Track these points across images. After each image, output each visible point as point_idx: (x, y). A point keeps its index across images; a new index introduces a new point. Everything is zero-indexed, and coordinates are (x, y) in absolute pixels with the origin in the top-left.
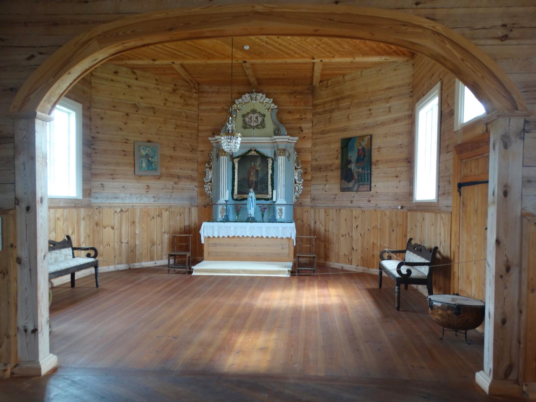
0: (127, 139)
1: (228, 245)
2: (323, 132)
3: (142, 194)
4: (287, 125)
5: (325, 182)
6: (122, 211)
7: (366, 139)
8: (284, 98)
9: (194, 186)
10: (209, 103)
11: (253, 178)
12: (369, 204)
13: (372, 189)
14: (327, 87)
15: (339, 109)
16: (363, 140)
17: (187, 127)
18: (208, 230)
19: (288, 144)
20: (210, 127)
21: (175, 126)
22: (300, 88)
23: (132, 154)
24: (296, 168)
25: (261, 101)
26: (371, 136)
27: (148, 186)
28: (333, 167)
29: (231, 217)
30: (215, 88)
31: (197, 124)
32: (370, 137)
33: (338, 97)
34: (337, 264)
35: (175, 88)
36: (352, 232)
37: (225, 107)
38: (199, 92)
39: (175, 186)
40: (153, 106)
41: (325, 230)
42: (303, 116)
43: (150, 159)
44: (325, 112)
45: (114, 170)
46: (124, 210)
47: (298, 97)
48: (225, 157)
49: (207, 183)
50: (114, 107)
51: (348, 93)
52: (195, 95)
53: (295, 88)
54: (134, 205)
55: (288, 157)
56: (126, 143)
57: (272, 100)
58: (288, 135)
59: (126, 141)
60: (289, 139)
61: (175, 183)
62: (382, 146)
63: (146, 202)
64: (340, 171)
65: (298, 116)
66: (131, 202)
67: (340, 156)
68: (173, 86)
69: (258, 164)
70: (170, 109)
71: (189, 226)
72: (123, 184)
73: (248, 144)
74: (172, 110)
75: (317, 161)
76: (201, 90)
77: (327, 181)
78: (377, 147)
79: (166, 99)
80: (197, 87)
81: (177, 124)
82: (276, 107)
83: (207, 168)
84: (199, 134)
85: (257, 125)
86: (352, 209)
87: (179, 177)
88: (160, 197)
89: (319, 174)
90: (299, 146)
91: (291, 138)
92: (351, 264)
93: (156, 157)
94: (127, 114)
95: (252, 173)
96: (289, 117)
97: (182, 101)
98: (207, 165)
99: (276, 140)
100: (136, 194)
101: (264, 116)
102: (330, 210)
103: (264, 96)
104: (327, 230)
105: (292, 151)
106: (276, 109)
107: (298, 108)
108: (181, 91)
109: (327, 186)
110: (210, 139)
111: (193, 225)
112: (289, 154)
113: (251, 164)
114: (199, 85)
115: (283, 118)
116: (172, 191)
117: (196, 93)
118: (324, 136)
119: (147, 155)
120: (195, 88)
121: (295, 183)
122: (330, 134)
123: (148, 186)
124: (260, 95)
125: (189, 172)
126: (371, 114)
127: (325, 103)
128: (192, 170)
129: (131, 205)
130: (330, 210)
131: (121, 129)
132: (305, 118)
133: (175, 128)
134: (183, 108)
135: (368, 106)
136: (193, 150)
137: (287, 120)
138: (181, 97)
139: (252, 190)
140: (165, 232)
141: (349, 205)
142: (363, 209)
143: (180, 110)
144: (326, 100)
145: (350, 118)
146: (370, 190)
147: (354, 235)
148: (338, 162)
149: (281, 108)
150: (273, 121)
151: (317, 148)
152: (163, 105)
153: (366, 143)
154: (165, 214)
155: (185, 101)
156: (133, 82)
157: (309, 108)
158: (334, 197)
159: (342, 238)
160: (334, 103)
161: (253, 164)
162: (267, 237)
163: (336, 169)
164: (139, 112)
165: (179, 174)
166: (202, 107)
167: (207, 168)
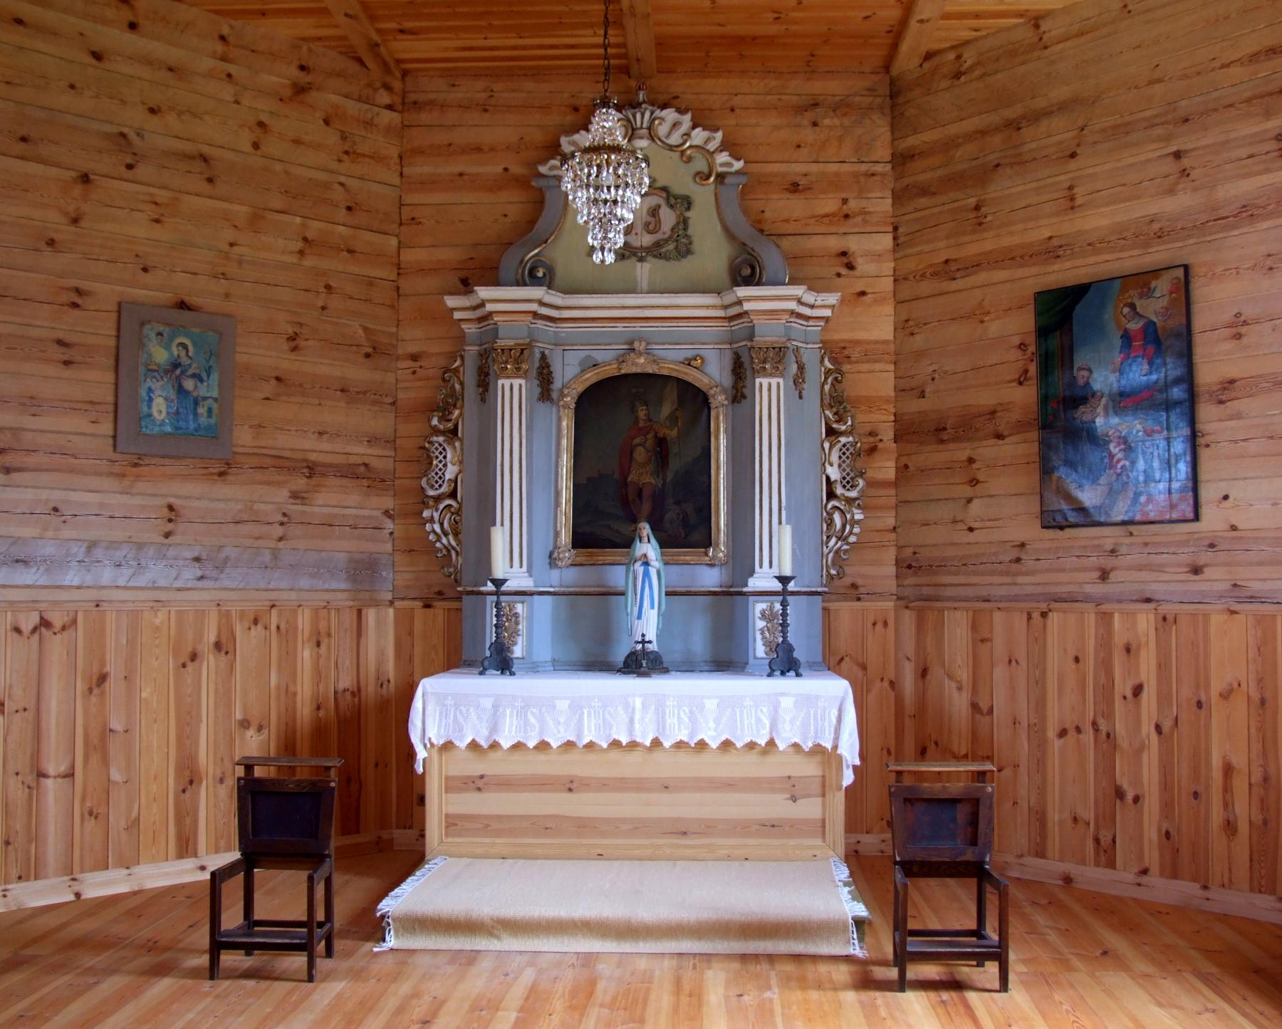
0: (78, 291)
1: (570, 785)
2: (947, 270)
3: (141, 546)
4: (786, 243)
5: (968, 491)
6: (45, 623)
7: (1162, 286)
8: (763, 128)
9: (378, 513)
10: (448, 150)
11: (643, 476)
12: (1197, 585)
13: (1205, 511)
14: (958, 75)
15: (1020, 162)
16: (1147, 293)
17: (350, 251)
18: (448, 714)
19: (798, 325)
20: (448, 255)
21: (300, 245)
22: (832, 87)
23: (111, 408)
24: (831, 432)
25: (675, 139)
26: (1186, 268)
27: (171, 508)
28: (1002, 423)
29: (1201, 617)
30: (472, 90)
31: (394, 242)
32: (1180, 273)
33: (1010, 113)
34: (1040, 862)
35: (304, 78)
36: (1109, 716)
37: (516, 169)
38: (405, 105)
39: (295, 508)
40: (206, 150)
41: (975, 707)
42: (853, 205)
43: (189, 384)
44: (955, 181)
45: (16, 431)
46: (57, 619)
47: (827, 122)
48: (516, 382)
49: (438, 499)
50: (23, 139)
51: (1061, 93)
52: (387, 117)
53: (818, 87)
54: (105, 595)
55: (799, 380)
56: (75, 305)
57: (719, 135)
58: (794, 281)
59: (77, 299)
60: (800, 302)
61: (295, 496)
62: (1249, 312)
63: (162, 583)
64: (1034, 435)
65: (829, 204)
66: (89, 580)
67: (1033, 369)
68: (294, 72)
69: (666, 410)
70: (278, 167)
71: (357, 692)
72: (57, 496)
73: (620, 327)
74: (286, 172)
75: (922, 395)
76: (412, 97)
77: (974, 482)
78: (1227, 316)
79: (261, 124)
80: (397, 85)
81: (310, 236)
82: (738, 165)
83: (436, 431)
84: (405, 285)
85: (658, 245)
86: (1104, 607)
87: (312, 470)
88: (226, 560)
89: (933, 455)
90: (840, 335)
91: (810, 298)
92: (1111, 864)
93: (215, 376)
94: (85, 179)
95: (640, 455)
96: (795, 207)
97: (331, 138)
98: (435, 422)
99: (747, 306)
100: (113, 545)
101: (687, 202)
102: (998, 616)
103: (687, 119)
104: (984, 706)
105: (811, 354)
106: (738, 173)
107: (833, 168)
108: (327, 98)
109: (976, 507)
110: (451, 302)
111: (370, 689)
112: (801, 368)
113: (633, 409)
114: (405, 73)
115: (768, 214)
116: (279, 531)
117: (390, 107)
118: (954, 285)
119: (176, 365)
120: (387, 87)
121: (831, 495)
122: (982, 277)
123: (171, 508)
124: (670, 115)
125: (360, 451)
126: (1184, 173)
127: (949, 145)
128: (372, 440)
129: (93, 595)
130: (998, 616)
131: (51, 243)
132: (863, 212)
133: (301, 252)
134: (334, 165)
135: (1167, 139)
136: (375, 352)
137: (787, 221)
138: (327, 122)
139: (646, 529)
140: (245, 724)
141: (1088, 589)
142: (1165, 608)
143: (322, 176)
144: (953, 129)
145: (1078, 202)
146: (1197, 518)
147: (1120, 729)
148: (1026, 396)
149: (755, 168)
150: (726, 229)
151: (919, 341)
152: (247, 147)
153: (1164, 302)
154: (248, 641)
155: (344, 138)
156: (114, 37)
157: (879, 168)
158: (1014, 554)
159: (1057, 743)
160: (997, 140)
161: (642, 414)
162: (727, 745)
163: (1021, 427)
164: (143, 171)
165: (313, 457)
166: (420, 169)
167: (436, 431)
